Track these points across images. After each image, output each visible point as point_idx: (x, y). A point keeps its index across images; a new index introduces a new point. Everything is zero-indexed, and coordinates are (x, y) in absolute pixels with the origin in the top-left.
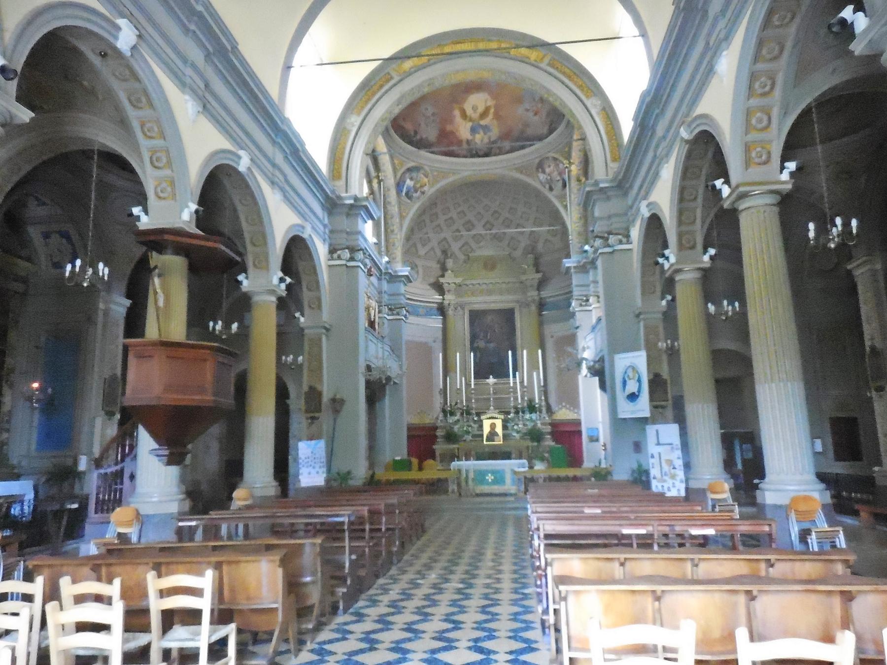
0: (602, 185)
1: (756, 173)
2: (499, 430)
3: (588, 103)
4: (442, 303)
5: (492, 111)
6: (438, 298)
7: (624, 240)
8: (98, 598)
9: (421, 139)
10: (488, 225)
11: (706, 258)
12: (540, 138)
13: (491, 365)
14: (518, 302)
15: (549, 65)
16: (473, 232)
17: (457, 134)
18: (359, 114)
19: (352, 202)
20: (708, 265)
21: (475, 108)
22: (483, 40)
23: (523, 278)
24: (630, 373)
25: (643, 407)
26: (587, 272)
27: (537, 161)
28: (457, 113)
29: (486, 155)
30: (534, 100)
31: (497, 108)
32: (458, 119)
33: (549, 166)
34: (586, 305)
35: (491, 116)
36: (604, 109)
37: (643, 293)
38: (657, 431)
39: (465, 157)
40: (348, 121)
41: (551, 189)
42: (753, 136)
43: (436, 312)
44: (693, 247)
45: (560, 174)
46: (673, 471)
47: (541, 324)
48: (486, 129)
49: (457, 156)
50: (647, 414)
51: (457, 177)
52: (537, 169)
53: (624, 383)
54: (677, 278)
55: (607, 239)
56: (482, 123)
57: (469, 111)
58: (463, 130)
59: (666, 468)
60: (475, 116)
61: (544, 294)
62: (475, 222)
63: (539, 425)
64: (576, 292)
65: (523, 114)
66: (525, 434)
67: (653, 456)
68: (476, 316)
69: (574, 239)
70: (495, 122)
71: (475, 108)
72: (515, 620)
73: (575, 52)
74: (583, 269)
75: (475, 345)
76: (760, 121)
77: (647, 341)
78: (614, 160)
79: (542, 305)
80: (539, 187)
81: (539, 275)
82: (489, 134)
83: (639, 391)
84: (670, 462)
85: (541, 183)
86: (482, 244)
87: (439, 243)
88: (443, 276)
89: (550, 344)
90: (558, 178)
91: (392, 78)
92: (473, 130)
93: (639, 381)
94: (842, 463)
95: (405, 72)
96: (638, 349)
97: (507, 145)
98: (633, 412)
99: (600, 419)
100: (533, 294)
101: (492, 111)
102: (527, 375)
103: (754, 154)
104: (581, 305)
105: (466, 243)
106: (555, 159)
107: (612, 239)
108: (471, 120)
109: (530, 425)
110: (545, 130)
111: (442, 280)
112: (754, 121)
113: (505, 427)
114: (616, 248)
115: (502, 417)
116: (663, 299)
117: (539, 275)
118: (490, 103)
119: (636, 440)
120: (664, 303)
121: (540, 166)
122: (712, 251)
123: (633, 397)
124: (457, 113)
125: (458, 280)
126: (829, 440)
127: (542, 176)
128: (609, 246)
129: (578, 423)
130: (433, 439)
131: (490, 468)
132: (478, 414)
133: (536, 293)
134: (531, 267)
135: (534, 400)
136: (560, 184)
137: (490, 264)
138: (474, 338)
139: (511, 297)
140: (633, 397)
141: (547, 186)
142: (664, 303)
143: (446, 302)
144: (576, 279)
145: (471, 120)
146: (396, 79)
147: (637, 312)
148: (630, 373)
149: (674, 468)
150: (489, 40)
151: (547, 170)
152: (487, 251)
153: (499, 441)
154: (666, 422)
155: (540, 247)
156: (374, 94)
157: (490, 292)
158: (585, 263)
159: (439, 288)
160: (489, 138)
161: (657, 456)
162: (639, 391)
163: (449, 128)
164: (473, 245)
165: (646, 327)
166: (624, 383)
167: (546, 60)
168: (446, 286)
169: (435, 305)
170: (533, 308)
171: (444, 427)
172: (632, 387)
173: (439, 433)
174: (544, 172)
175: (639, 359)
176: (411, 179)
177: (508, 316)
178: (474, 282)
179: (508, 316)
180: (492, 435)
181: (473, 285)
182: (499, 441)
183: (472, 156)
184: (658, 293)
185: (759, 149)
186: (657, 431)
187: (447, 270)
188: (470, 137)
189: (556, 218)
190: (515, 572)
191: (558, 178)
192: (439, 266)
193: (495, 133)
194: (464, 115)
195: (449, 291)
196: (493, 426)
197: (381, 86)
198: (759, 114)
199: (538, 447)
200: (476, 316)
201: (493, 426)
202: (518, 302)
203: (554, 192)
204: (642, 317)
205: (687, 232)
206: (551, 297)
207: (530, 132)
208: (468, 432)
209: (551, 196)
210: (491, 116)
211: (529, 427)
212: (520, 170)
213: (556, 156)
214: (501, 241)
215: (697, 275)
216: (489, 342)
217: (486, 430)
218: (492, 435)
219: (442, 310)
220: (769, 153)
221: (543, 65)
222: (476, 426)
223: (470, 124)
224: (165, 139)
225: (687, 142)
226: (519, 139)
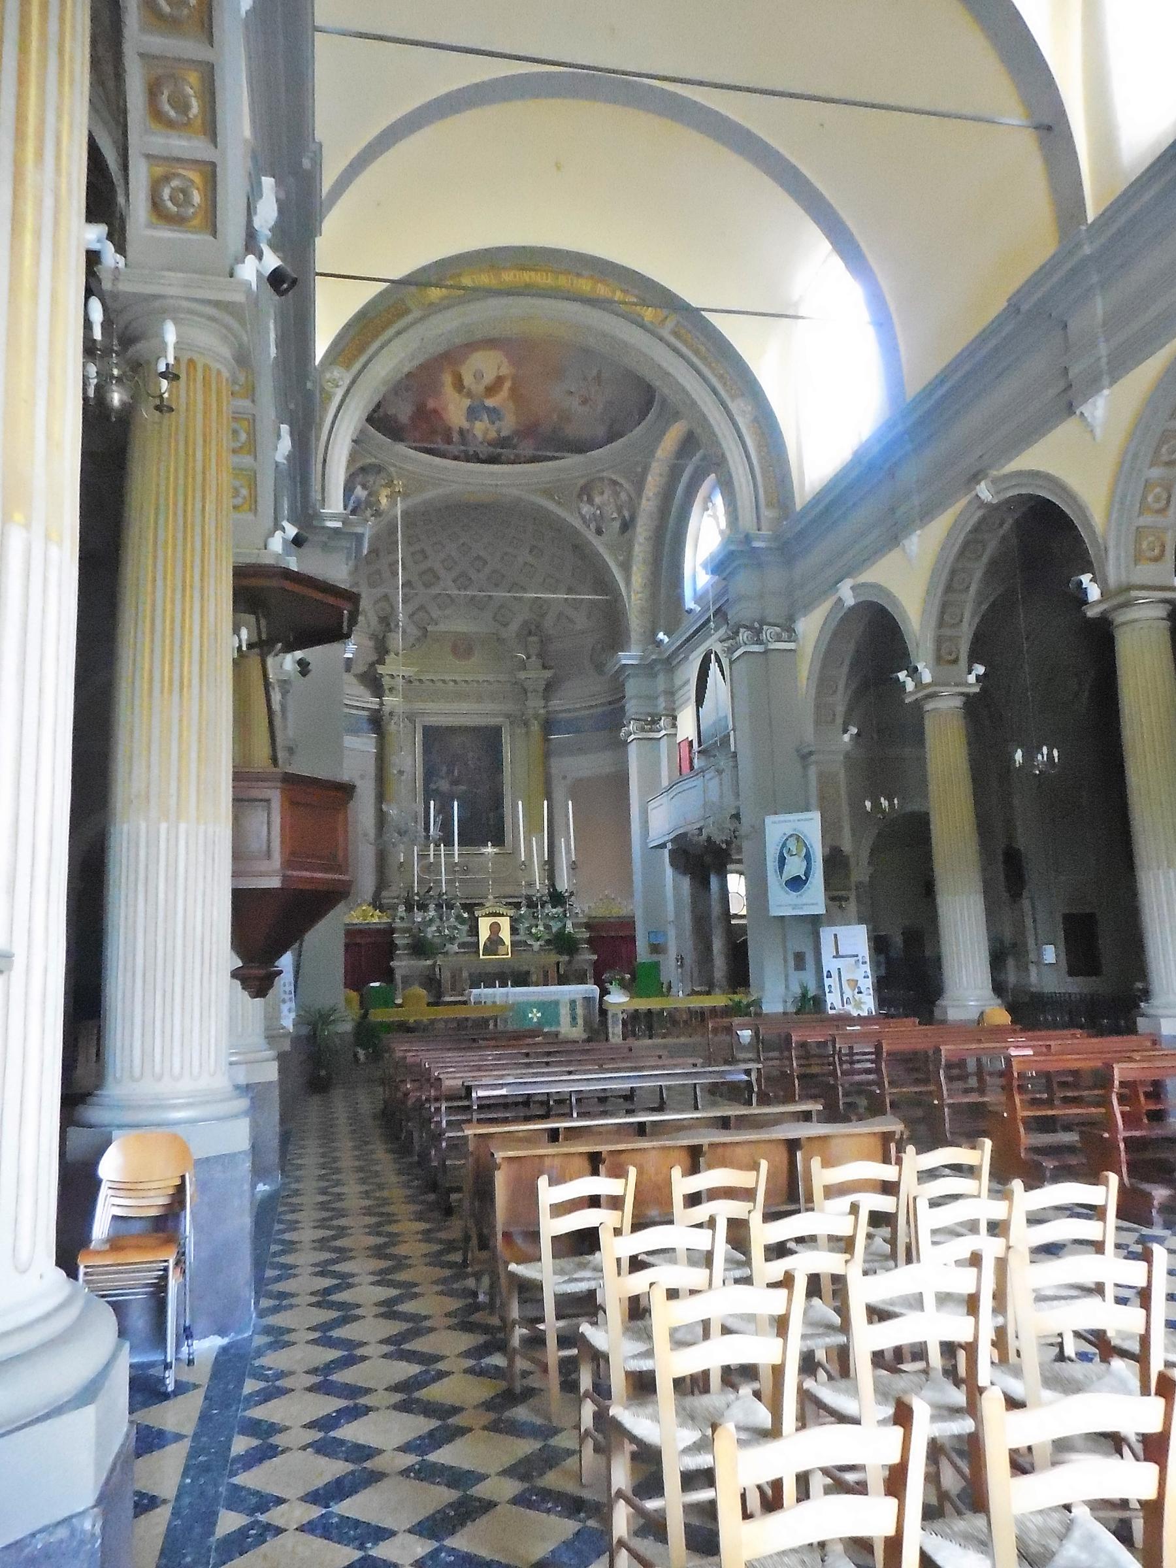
0: (756, 544)
1: (1146, 573)
2: (505, 935)
3: (732, 406)
4: (378, 711)
5: (507, 385)
6: (372, 702)
7: (785, 635)
8: (958, 1169)
9: (386, 415)
10: (463, 581)
11: (972, 679)
12: (580, 447)
13: (485, 825)
14: (508, 716)
15: (676, 334)
16: (435, 590)
17: (445, 416)
18: (348, 367)
19: (339, 525)
20: (977, 690)
21: (478, 376)
22: (567, 272)
23: (522, 675)
24: (792, 845)
25: (814, 899)
26: (655, 676)
27: (582, 482)
28: (447, 379)
29: (493, 460)
30: (585, 379)
31: (514, 378)
32: (448, 390)
33: (602, 493)
34: (651, 731)
35: (505, 392)
36: (756, 420)
37: (817, 723)
38: (836, 936)
39: (456, 458)
40: (328, 376)
41: (599, 532)
42: (1147, 520)
43: (365, 726)
44: (955, 661)
45: (620, 511)
46: (858, 996)
47: (547, 755)
48: (494, 414)
49: (443, 455)
50: (820, 910)
51: (440, 491)
52: (580, 496)
53: (782, 861)
54: (929, 706)
55: (760, 631)
56: (490, 403)
57: (468, 380)
58: (455, 411)
59: (848, 993)
60: (479, 389)
61: (555, 704)
62: (442, 573)
63: (569, 928)
64: (632, 707)
65: (572, 402)
66: (548, 942)
67: (829, 976)
68: (433, 736)
69: (635, 622)
70: (511, 405)
71: (478, 376)
72: (322, 1274)
73: (723, 324)
74: (648, 669)
75: (433, 786)
76: (1157, 499)
77: (822, 798)
78: (769, 505)
79: (549, 726)
80: (577, 523)
81: (548, 674)
82: (498, 423)
83: (807, 874)
84: (854, 983)
85: (583, 517)
86: (447, 612)
87: (376, 603)
88: (381, 661)
89: (559, 792)
90: (615, 515)
91: (407, 311)
92: (472, 413)
93: (808, 857)
94: (1079, 979)
95: (431, 304)
96: (807, 809)
97: (526, 448)
98: (795, 907)
99: (671, 916)
100: (535, 704)
101: (507, 385)
102: (540, 841)
103: (1144, 545)
104: (643, 730)
105: (422, 608)
106: (615, 483)
107: (768, 632)
108: (469, 395)
109: (555, 926)
110: (601, 431)
111: (381, 669)
112: (1150, 499)
113: (514, 931)
114: (771, 646)
115: (512, 913)
116: (845, 731)
117: (548, 674)
118: (505, 370)
119: (798, 950)
120: (846, 738)
121: (586, 492)
122: (980, 669)
123: (796, 883)
124: (447, 379)
125: (409, 671)
126: (1062, 947)
127: (586, 509)
128: (759, 642)
129: (628, 924)
130: (389, 950)
131: (533, 999)
132: (469, 908)
133: (542, 703)
134: (534, 658)
135: (413, 888)
136: (617, 525)
137: (462, 648)
138: (430, 774)
139: (490, 707)
140: (796, 883)
141: (593, 526)
142: (846, 738)
143: (386, 710)
144: (632, 687)
145: (469, 395)
146: (416, 314)
147: (806, 750)
148: (792, 845)
149: (860, 992)
150: (578, 275)
151: (598, 500)
152: (460, 625)
153: (506, 953)
154: (848, 923)
155: (548, 623)
156: (375, 336)
157: (461, 696)
158: (655, 660)
159: (374, 683)
160: (498, 432)
161: (835, 974)
162: (807, 874)
163: (431, 404)
164: (435, 613)
165: (821, 775)
166: (782, 861)
167: (670, 324)
168: (386, 681)
169: (366, 713)
170: (535, 727)
171: (408, 930)
172: (795, 867)
173: (400, 940)
174: (590, 501)
175: (810, 825)
176: (364, 487)
177: (490, 739)
178: (447, 678)
179: (490, 739)
180: (495, 942)
181: (444, 681)
182: (506, 953)
183: (468, 459)
184: (839, 721)
185: (1151, 539)
186: (836, 936)
187: (387, 652)
188: (466, 425)
189: (603, 583)
190: (324, 1192)
191: (615, 515)
192: (371, 644)
193: (508, 424)
194: (459, 385)
195: (391, 690)
196: (495, 928)
197: (389, 323)
198: (1158, 490)
199: (570, 962)
200: (433, 736)
201: (495, 928)
202: (508, 716)
203: (605, 538)
204: (813, 758)
205: (951, 639)
206: (565, 711)
207: (571, 431)
208: (452, 939)
209: (599, 545)
210: (505, 392)
211: (554, 930)
212: (548, 493)
213: (614, 477)
214: (482, 609)
215: (958, 702)
216: (455, 782)
217: (484, 934)
218: (495, 942)
219: (377, 722)
220: (1163, 546)
221: (665, 333)
222: (465, 928)
223: (467, 402)
224: (253, 401)
225: (982, 504)
226: (543, 440)
